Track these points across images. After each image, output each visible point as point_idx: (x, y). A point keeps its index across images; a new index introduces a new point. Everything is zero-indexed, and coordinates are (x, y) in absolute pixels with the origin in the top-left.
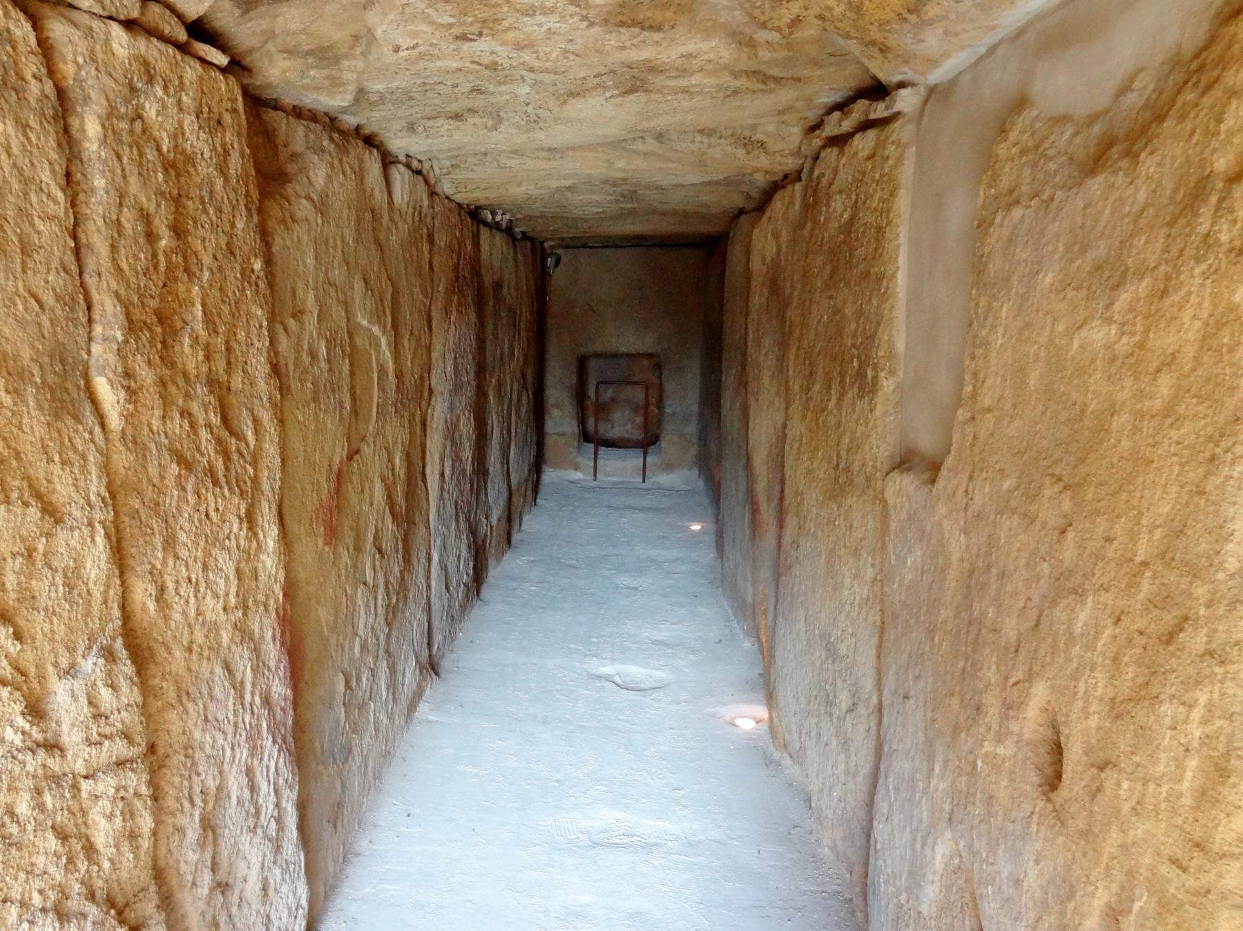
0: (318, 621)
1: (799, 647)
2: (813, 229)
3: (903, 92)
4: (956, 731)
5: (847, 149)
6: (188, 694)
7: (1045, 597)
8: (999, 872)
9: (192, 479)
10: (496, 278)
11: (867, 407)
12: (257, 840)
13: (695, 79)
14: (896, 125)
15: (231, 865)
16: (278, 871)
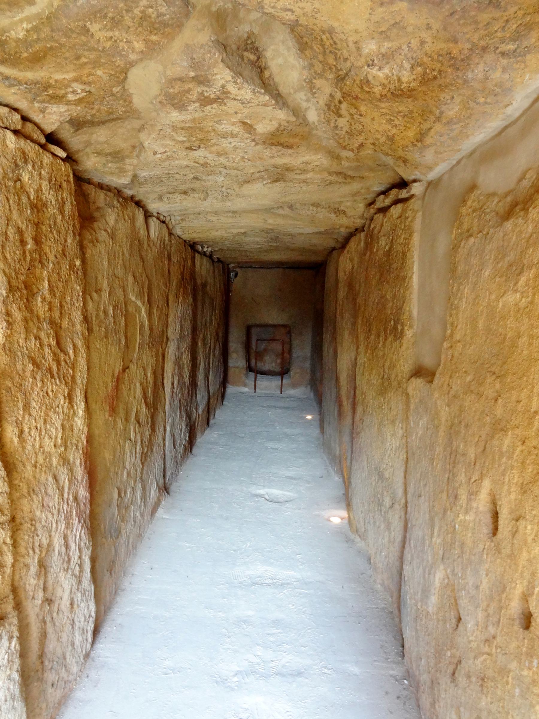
0: (105, 458)
1: (363, 475)
2: (370, 255)
3: (415, 184)
4: (445, 511)
5: (387, 214)
6: (33, 490)
7: (488, 434)
8: (467, 583)
9: (40, 374)
10: (203, 281)
11: (398, 345)
12: (68, 576)
13: (310, 175)
14: (412, 201)
15: (54, 589)
16: (79, 595)
